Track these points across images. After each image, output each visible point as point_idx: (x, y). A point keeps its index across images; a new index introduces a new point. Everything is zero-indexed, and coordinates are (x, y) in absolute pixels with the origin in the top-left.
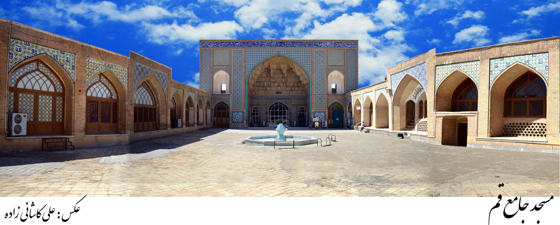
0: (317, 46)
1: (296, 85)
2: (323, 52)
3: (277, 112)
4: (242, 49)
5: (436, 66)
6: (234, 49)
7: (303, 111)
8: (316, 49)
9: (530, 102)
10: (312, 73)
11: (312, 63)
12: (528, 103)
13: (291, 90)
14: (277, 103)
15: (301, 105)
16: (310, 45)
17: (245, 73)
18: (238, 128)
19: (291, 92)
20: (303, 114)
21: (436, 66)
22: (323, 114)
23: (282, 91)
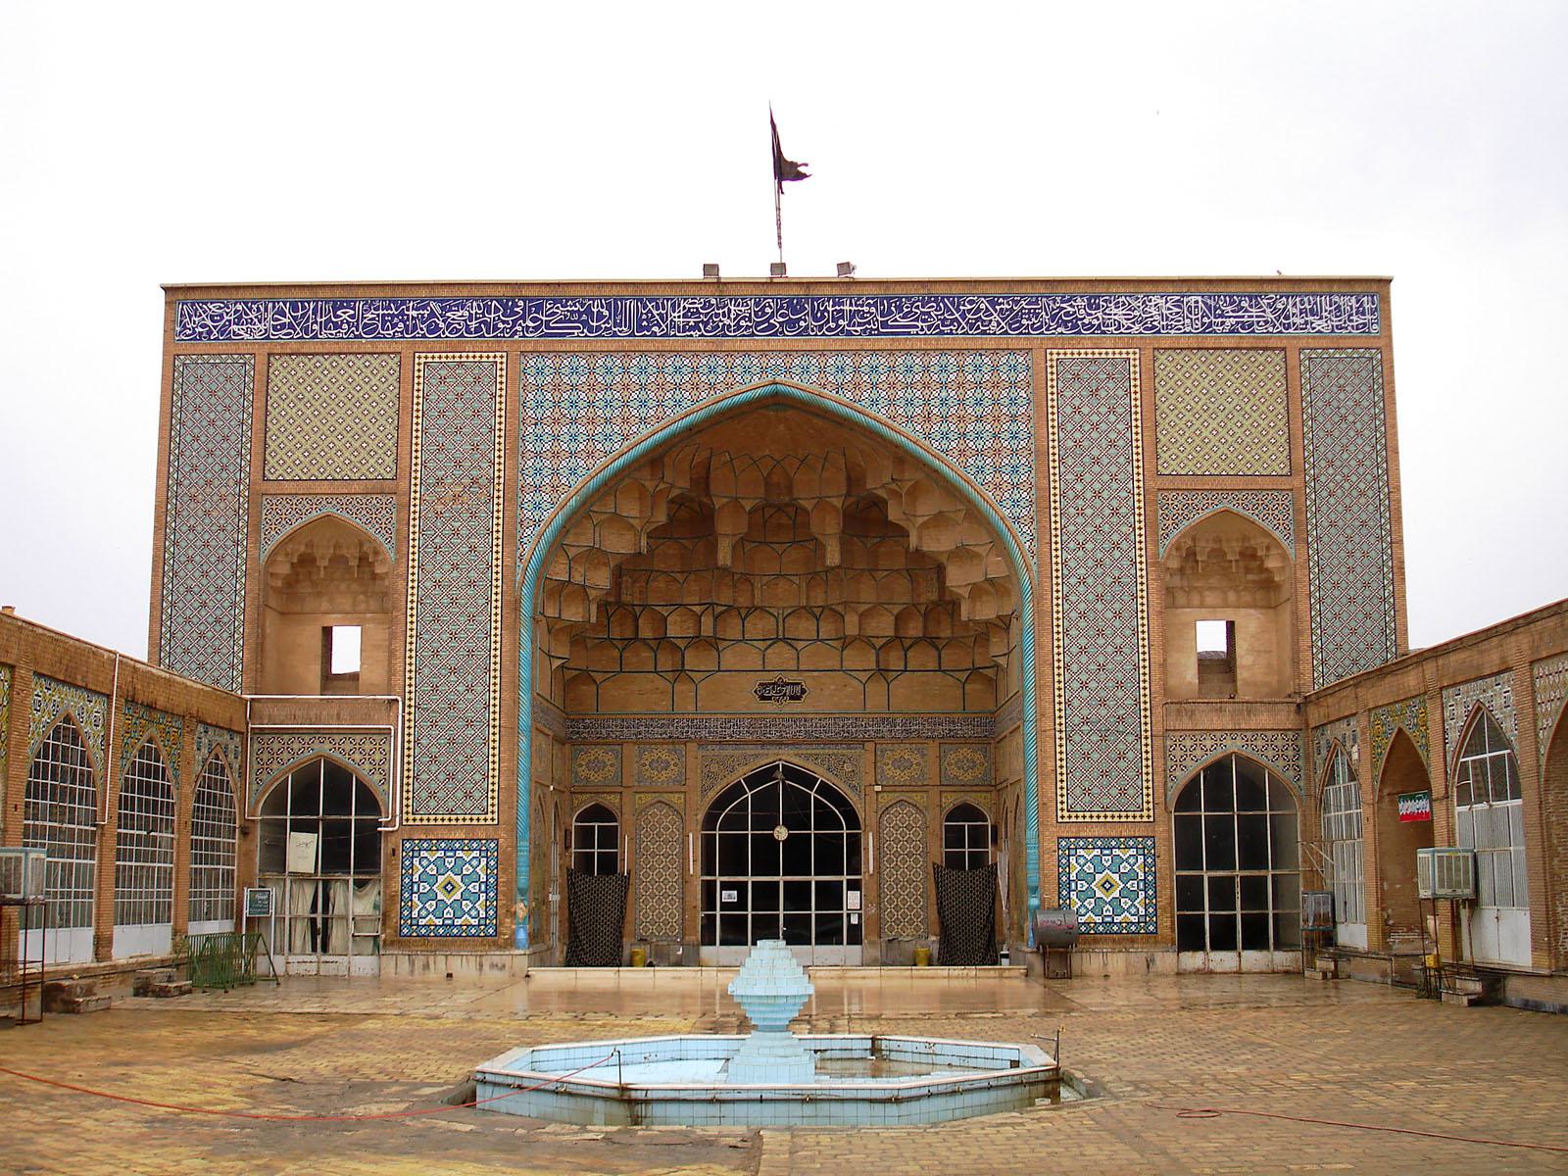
0: (1074, 325)
1: (914, 629)
2: (1118, 372)
3: (766, 848)
4: (492, 357)
5: (1532, 663)
6: (428, 357)
7: (978, 837)
8: (1063, 353)
9: (721, 882)
10: (1043, 535)
11: (1042, 454)
12: (712, 878)
13: (882, 671)
14: (768, 774)
15: (964, 787)
16: (1014, 321)
17: (511, 538)
18: (591, 966)
19: (877, 689)
20: (978, 860)
21: (1532, 663)
22: (1132, 860)
23: (807, 681)
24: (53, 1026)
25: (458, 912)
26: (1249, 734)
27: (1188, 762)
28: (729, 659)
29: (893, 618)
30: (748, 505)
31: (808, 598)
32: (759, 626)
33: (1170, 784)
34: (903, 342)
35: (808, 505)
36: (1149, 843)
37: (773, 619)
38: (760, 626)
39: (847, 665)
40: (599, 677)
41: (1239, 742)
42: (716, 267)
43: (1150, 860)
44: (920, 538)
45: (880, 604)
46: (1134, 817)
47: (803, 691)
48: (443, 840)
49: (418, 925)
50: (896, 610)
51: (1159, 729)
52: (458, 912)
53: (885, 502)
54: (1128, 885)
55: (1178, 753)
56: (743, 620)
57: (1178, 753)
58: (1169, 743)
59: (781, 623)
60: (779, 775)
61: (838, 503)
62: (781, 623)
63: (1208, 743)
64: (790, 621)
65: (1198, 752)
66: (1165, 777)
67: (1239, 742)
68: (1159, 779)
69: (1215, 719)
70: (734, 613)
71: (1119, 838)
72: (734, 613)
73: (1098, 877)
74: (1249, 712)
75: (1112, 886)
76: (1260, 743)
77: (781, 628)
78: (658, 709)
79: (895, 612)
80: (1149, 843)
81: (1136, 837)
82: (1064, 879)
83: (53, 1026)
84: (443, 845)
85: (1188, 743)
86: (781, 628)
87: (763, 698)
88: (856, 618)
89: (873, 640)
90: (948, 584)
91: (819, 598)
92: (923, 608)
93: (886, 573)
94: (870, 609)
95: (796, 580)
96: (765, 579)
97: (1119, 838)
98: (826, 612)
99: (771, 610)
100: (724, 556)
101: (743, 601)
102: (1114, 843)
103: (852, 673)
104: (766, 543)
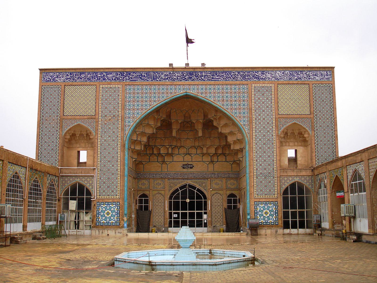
0: (258, 78)
1: (220, 151)
2: (269, 90)
3: (184, 204)
4: (118, 86)
5: (368, 159)
6: (103, 86)
7: (235, 201)
8: (256, 85)
9: (173, 212)
10: (251, 129)
11: (250, 109)
12: (171, 211)
13: (212, 162)
14: (185, 186)
15: (232, 189)
16: (244, 77)
17: (123, 130)
18: (142, 232)
19: (211, 166)
20: (235, 207)
21: (368, 159)
22: (272, 207)
23: (194, 164)
24: (13, 247)
25: (110, 220)
26: (300, 177)
27: (286, 183)
28: (175, 159)
29: (215, 149)
30: (180, 122)
31: (194, 144)
32: (182, 151)
33: (281, 189)
34: (217, 82)
35: (194, 121)
36: (276, 203)
37: (186, 149)
38: (183, 151)
39: (204, 160)
40: (144, 163)
41: (298, 179)
42: (172, 64)
43: (276, 207)
44: (221, 130)
45: (212, 145)
46: (273, 197)
47: (193, 166)
48: (107, 202)
49: (101, 223)
50: (215, 147)
51: (279, 175)
52: (110, 220)
53: (213, 121)
54: (271, 213)
55: (283, 181)
56: (179, 149)
57: (283, 181)
58: (281, 179)
59: (188, 150)
60: (187, 186)
61: (201, 121)
62: (188, 150)
63: (291, 179)
64: (190, 149)
65: (288, 181)
66: (280, 187)
67: (298, 179)
68: (279, 187)
69: (292, 173)
70: (177, 147)
71: (269, 202)
72: (177, 147)
73: (264, 211)
74: (300, 171)
75: (267, 213)
76: (303, 179)
77: (188, 151)
78: (158, 171)
79: (215, 147)
80: (276, 203)
81: (273, 202)
82: (256, 211)
83: (13, 247)
84: (107, 203)
85: (286, 179)
86: (188, 151)
87: (183, 168)
88: (206, 149)
89: (210, 154)
90: (228, 141)
91: (197, 144)
92: (222, 146)
93: (213, 138)
94: (209, 147)
95: (191, 139)
96: (184, 139)
97: (269, 202)
98: (199, 147)
99: (185, 147)
100: (174, 134)
101: (179, 145)
102: (268, 203)
103: (205, 162)
104: (184, 131)
